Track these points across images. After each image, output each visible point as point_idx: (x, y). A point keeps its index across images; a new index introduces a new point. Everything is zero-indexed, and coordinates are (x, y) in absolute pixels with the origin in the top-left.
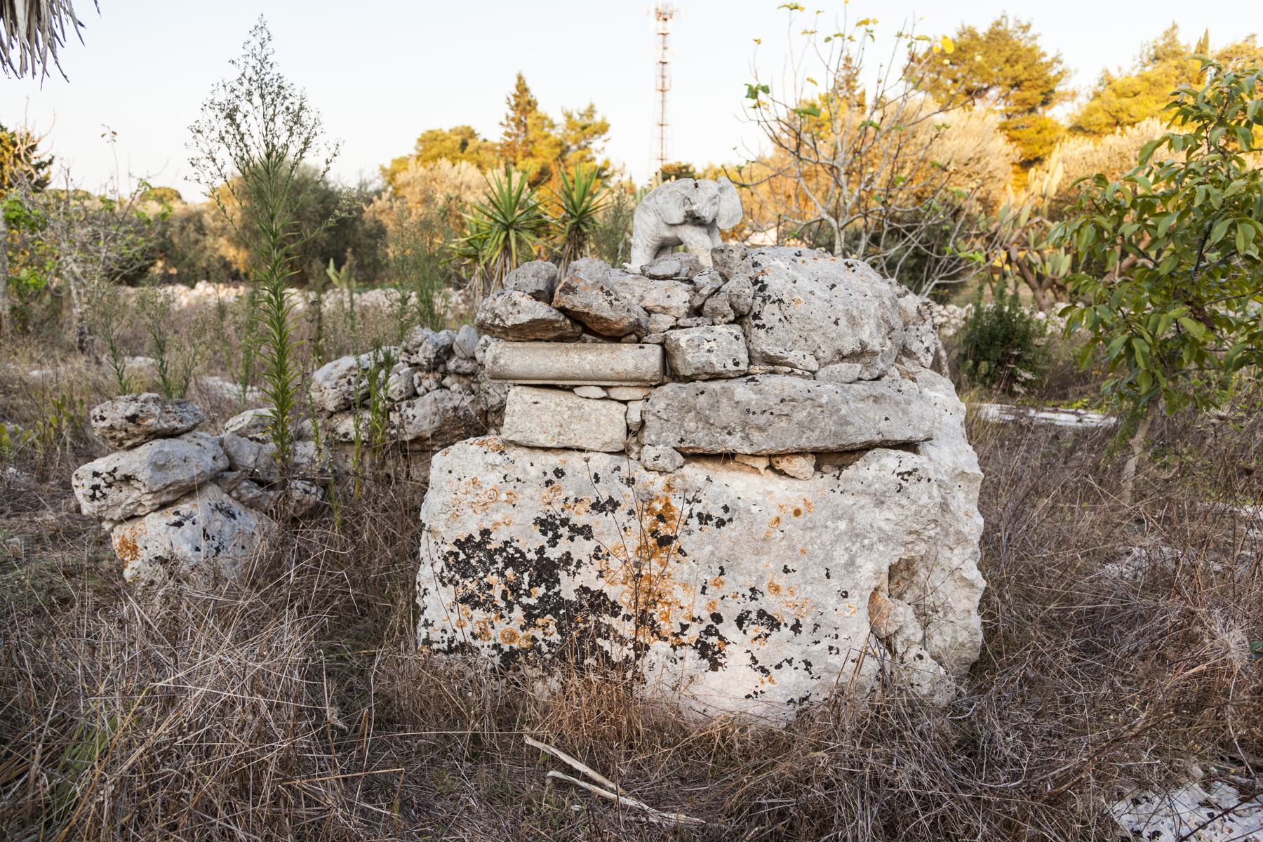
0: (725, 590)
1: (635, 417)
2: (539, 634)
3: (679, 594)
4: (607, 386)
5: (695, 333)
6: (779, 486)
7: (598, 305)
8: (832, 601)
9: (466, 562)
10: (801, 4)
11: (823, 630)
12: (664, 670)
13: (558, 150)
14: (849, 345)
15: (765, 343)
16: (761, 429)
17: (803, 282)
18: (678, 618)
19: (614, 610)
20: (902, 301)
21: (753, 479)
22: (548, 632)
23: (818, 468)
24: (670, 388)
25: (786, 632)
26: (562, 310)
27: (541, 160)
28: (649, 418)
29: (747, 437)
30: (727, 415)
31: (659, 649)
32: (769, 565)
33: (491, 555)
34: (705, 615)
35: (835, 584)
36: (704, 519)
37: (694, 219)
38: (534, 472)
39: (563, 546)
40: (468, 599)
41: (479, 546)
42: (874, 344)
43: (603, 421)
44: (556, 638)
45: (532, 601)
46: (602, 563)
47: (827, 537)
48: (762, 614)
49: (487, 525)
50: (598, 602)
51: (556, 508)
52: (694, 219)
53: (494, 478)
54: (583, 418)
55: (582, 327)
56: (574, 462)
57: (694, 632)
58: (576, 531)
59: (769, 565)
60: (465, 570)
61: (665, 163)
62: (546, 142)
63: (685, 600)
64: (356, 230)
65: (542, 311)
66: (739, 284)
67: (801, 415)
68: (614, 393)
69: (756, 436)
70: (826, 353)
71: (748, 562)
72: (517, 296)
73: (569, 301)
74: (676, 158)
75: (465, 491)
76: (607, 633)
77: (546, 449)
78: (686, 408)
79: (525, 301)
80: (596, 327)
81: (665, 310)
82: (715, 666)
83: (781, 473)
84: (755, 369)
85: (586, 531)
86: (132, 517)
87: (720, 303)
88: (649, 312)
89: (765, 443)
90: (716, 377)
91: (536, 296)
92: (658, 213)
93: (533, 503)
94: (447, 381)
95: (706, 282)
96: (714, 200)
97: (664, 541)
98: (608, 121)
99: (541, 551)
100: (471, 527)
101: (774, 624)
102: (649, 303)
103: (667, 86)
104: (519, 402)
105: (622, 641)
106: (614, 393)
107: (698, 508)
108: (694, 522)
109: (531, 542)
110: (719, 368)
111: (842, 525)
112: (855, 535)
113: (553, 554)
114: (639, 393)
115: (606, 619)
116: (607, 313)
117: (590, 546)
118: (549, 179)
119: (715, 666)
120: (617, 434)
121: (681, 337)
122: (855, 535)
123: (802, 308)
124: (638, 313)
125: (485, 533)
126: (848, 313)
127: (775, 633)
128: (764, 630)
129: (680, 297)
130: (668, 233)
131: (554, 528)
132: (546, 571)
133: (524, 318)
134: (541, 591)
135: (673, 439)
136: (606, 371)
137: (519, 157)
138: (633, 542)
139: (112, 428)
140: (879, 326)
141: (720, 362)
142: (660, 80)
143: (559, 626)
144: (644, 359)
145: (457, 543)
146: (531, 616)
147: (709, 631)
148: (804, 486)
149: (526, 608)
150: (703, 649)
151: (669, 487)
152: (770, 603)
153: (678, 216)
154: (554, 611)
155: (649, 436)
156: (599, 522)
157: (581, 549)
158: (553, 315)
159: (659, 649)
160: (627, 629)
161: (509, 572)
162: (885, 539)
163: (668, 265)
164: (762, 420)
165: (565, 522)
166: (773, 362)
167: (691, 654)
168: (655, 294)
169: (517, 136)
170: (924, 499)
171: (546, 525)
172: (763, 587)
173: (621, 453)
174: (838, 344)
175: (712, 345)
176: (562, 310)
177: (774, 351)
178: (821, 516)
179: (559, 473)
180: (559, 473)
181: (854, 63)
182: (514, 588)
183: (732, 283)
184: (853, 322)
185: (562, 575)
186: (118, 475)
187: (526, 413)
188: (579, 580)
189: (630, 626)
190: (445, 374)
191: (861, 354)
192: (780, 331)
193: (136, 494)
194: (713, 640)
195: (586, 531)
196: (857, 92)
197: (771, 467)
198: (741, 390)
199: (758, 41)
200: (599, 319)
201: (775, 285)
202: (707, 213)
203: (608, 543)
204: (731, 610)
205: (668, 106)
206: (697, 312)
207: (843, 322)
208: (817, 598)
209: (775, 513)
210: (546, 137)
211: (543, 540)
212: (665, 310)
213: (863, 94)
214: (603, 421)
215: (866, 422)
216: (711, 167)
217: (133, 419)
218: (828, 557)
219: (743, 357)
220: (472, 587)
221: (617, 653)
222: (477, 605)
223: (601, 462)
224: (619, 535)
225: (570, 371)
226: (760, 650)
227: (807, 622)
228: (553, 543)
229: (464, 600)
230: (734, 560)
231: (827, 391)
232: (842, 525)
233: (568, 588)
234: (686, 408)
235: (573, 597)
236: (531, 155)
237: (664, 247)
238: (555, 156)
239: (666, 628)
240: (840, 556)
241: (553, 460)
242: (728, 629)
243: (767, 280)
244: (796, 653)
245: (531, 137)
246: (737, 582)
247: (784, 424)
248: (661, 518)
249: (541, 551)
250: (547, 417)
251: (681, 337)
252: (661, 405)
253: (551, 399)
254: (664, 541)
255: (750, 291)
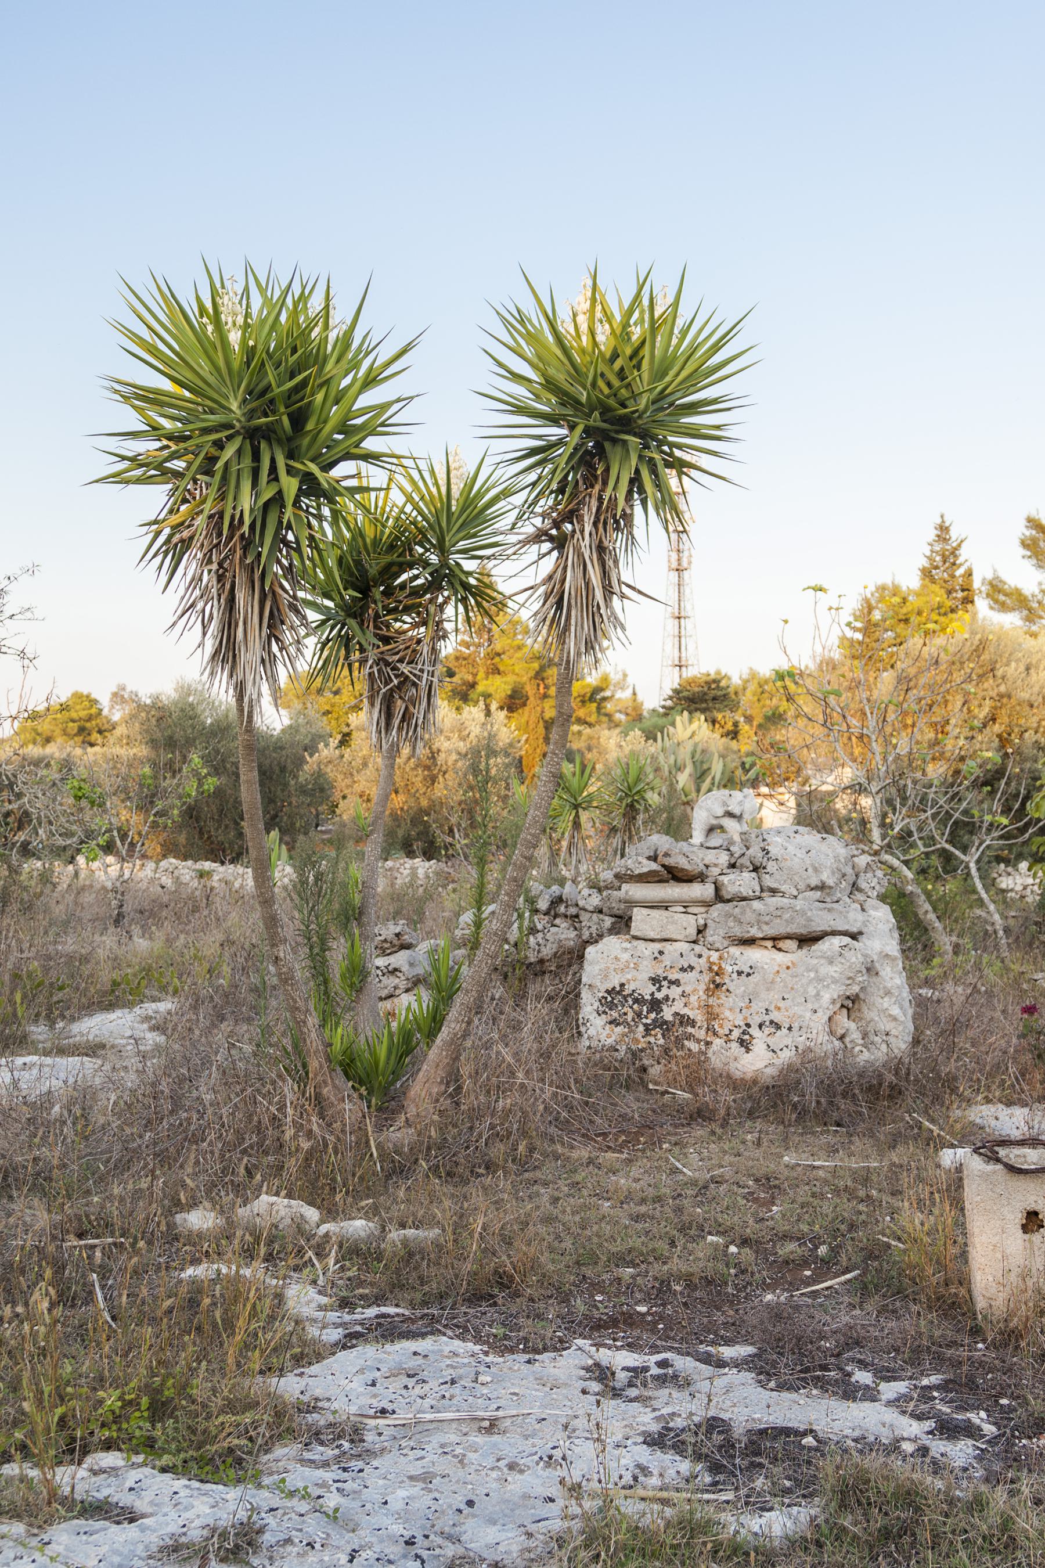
0: (752, 1010)
1: (701, 922)
2: (652, 1040)
3: (727, 1013)
4: (686, 906)
5: (732, 877)
6: (779, 956)
7: (682, 863)
8: (808, 1014)
9: (612, 1002)
10: (825, 586)
11: (804, 1030)
12: (723, 1055)
13: (536, 665)
14: (814, 882)
15: (769, 882)
16: (767, 923)
17: (791, 849)
18: (728, 1026)
19: (692, 1023)
20: (856, 859)
21: (766, 952)
22: (658, 1039)
23: (800, 947)
24: (720, 906)
25: (785, 1031)
26: (663, 866)
27: (511, 679)
28: (710, 922)
29: (760, 928)
30: (749, 916)
31: (718, 1042)
32: (774, 996)
33: (625, 997)
34: (742, 1024)
35: (810, 1006)
36: (740, 973)
37: (730, 814)
38: (647, 953)
39: (665, 991)
40: (613, 1022)
41: (619, 993)
42: (830, 882)
43: (685, 924)
44: (661, 1041)
45: (649, 1021)
46: (686, 999)
47: (804, 981)
48: (772, 1022)
49: (623, 981)
50: (684, 1021)
51: (660, 972)
52: (730, 814)
53: (626, 956)
54: (674, 923)
55: (675, 875)
56: (667, 947)
57: (736, 1033)
58: (672, 982)
59: (774, 996)
60: (612, 1006)
61: (690, 673)
62: (519, 655)
63: (731, 1017)
64: (286, 785)
65: (654, 866)
66: (755, 851)
67: (787, 916)
68: (690, 910)
69: (765, 927)
70: (802, 886)
71: (763, 995)
72: (640, 859)
73: (667, 861)
74: (704, 664)
75: (608, 962)
76: (690, 1037)
77: (652, 940)
78: (728, 915)
79: (645, 861)
80: (680, 875)
81: (716, 865)
82: (748, 1050)
83: (780, 950)
84: (764, 895)
85: (677, 983)
86: (391, 996)
87: (745, 861)
88: (707, 867)
89: (770, 931)
90: (744, 899)
91: (649, 858)
92: (708, 810)
93: (648, 969)
94: (557, 921)
95: (737, 849)
96: (740, 803)
97: (718, 986)
98: (990, 576)
99: (652, 994)
100: (615, 982)
101: (778, 1027)
102: (707, 862)
103: (685, 564)
104: (639, 915)
105: (698, 1041)
106: (690, 910)
107: (736, 968)
108: (735, 975)
109: (647, 991)
110: (745, 894)
111: (812, 975)
112: (820, 980)
113: (659, 996)
114: (703, 909)
115: (690, 1030)
116: (687, 867)
117: (679, 990)
118: (524, 705)
119: (748, 1050)
120: (692, 931)
121: (725, 879)
122: (820, 980)
123: (788, 863)
124: (702, 867)
125: (622, 985)
126: (812, 865)
127: (779, 1033)
128: (773, 1030)
129: (724, 858)
130: (714, 822)
131: (659, 982)
132: (655, 1005)
133: (645, 870)
134: (653, 1015)
135: (722, 932)
136: (686, 897)
137: (481, 675)
138: (702, 987)
139: (385, 941)
140: (833, 873)
141: (746, 892)
142: (674, 556)
143: (663, 1035)
144: (704, 891)
145: (607, 991)
146: (647, 1029)
147: (744, 1033)
148: (792, 955)
149: (645, 1025)
150: (742, 1042)
151: (721, 958)
152: (775, 1016)
153: (720, 812)
154: (660, 1026)
155: (709, 932)
156: (682, 977)
157: (675, 992)
158: (659, 868)
159: (718, 1042)
160: (701, 1034)
161: (635, 1006)
162: (835, 981)
163: (716, 840)
164: (767, 918)
165: (665, 978)
166: (773, 891)
167: (735, 1045)
168: (710, 857)
169: (479, 645)
170: (854, 959)
171: (655, 980)
172: (772, 1008)
173: (694, 942)
174: (808, 881)
175: (742, 882)
176: (663, 866)
177: (774, 885)
178: (800, 970)
179: (661, 953)
180: (661, 953)
181: (954, 534)
182: (639, 1015)
183: (751, 851)
184: (816, 870)
185: (664, 1007)
186: (390, 968)
187: (643, 921)
188: (674, 1009)
189: (703, 1032)
190: (556, 916)
191: (822, 887)
192: (777, 876)
193: (397, 981)
194: (747, 1037)
195: (677, 983)
196: (960, 572)
197: (774, 947)
198: (756, 904)
199: (786, 622)
200: (683, 870)
201: (774, 851)
202: (737, 811)
203: (688, 989)
204: (755, 1021)
205: (687, 590)
206: (733, 866)
207: (810, 870)
208: (800, 1013)
209: (777, 968)
210: (519, 648)
211: (654, 989)
212: (716, 865)
213: (969, 574)
214: (685, 924)
215: (822, 921)
216: (753, 675)
217: (398, 935)
218: (805, 991)
219: (758, 888)
220: (615, 1014)
221: (694, 1047)
222: (618, 1024)
223: (683, 947)
224: (695, 984)
225: (667, 898)
226: (771, 1041)
227: (795, 1026)
228: (659, 990)
229: (611, 1023)
230: (756, 994)
231: (799, 904)
232: (812, 975)
233: (667, 1014)
234: (728, 915)
235: (670, 1018)
236: (496, 671)
237: (711, 830)
238: (532, 673)
239: (721, 1032)
240: (812, 991)
241: (658, 946)
242: (754, 1031)
243: (769, 848)
244: (788, 1041)
245: (498, 647)
246: (758, 1006)
247: (778, 921)
248: (717, 974)
249: (652, 994)
250: (654, 922)
251: (725, 879)
252: (715, 914)
253: (655, 913)
254: (718, 986)
255: (760, 854)
